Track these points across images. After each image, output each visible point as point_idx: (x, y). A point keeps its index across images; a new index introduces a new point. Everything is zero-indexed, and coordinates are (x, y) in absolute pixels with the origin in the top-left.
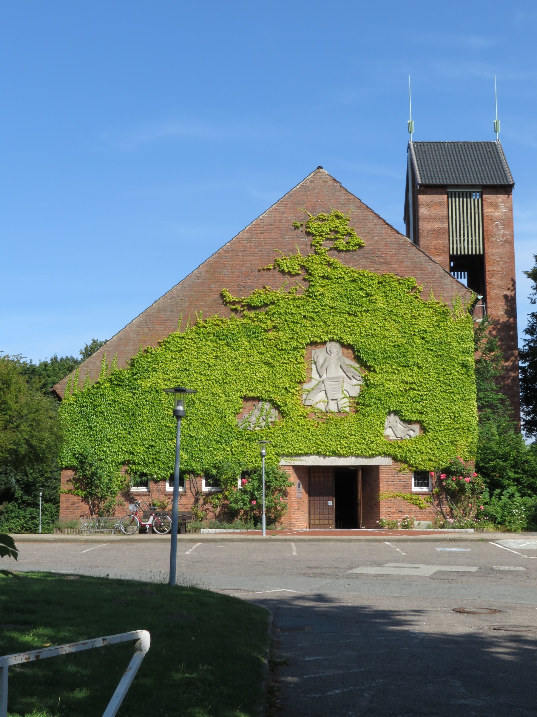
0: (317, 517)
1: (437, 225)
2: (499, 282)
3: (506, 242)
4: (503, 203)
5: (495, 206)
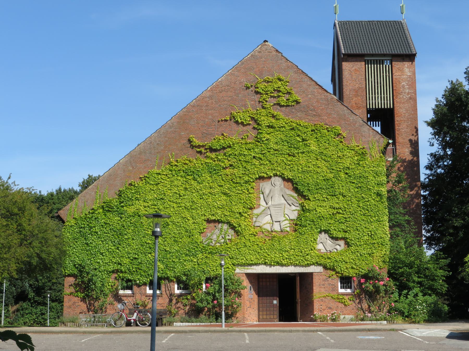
0: (265, 313)
1: (357, 86)
2: (406, 130)
3: (410, 98)
4: (408, 68)
5: (402, 71)
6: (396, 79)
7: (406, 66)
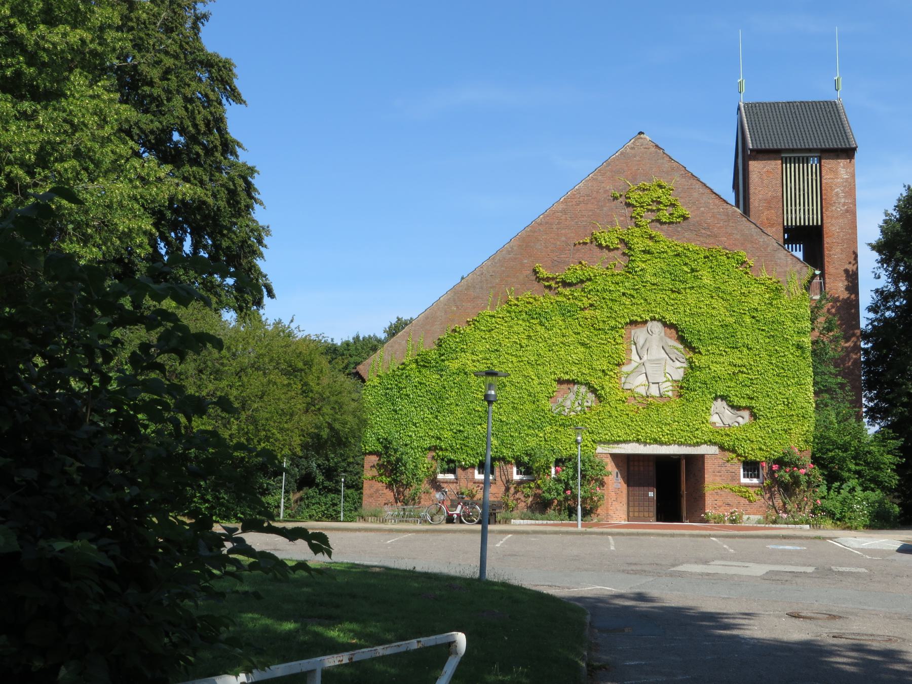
0: (637, 509)
2: (839, 256)
3: (847, 211)
6: (827, 183)
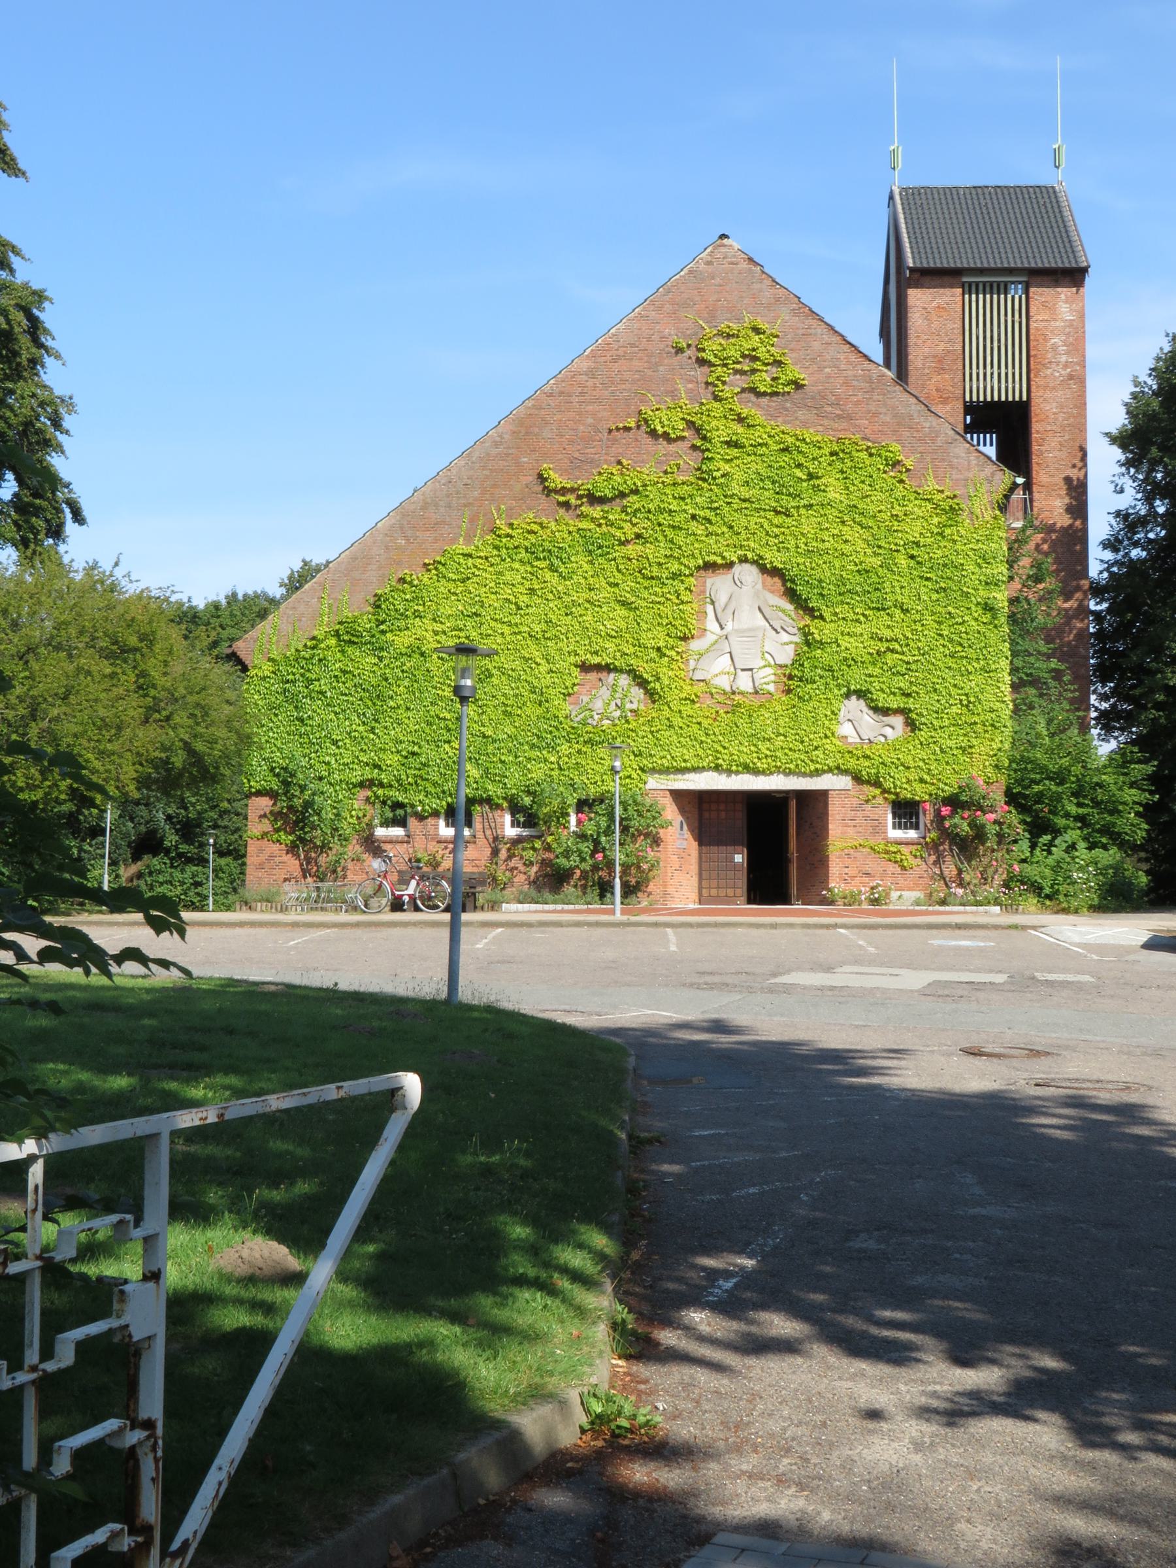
0: (714, 883)
1: (942, 346)
3: (1071, 377)
4: (1066, 302)
5: (1052, 309)
6: (1037, 329)
7: (1063, 296)
